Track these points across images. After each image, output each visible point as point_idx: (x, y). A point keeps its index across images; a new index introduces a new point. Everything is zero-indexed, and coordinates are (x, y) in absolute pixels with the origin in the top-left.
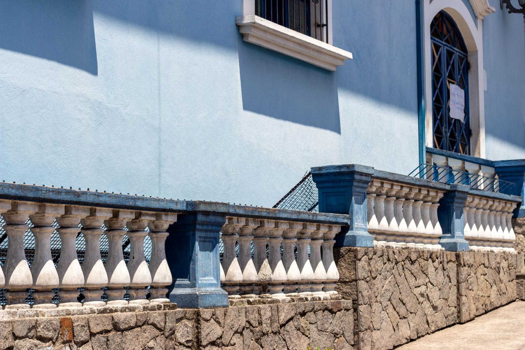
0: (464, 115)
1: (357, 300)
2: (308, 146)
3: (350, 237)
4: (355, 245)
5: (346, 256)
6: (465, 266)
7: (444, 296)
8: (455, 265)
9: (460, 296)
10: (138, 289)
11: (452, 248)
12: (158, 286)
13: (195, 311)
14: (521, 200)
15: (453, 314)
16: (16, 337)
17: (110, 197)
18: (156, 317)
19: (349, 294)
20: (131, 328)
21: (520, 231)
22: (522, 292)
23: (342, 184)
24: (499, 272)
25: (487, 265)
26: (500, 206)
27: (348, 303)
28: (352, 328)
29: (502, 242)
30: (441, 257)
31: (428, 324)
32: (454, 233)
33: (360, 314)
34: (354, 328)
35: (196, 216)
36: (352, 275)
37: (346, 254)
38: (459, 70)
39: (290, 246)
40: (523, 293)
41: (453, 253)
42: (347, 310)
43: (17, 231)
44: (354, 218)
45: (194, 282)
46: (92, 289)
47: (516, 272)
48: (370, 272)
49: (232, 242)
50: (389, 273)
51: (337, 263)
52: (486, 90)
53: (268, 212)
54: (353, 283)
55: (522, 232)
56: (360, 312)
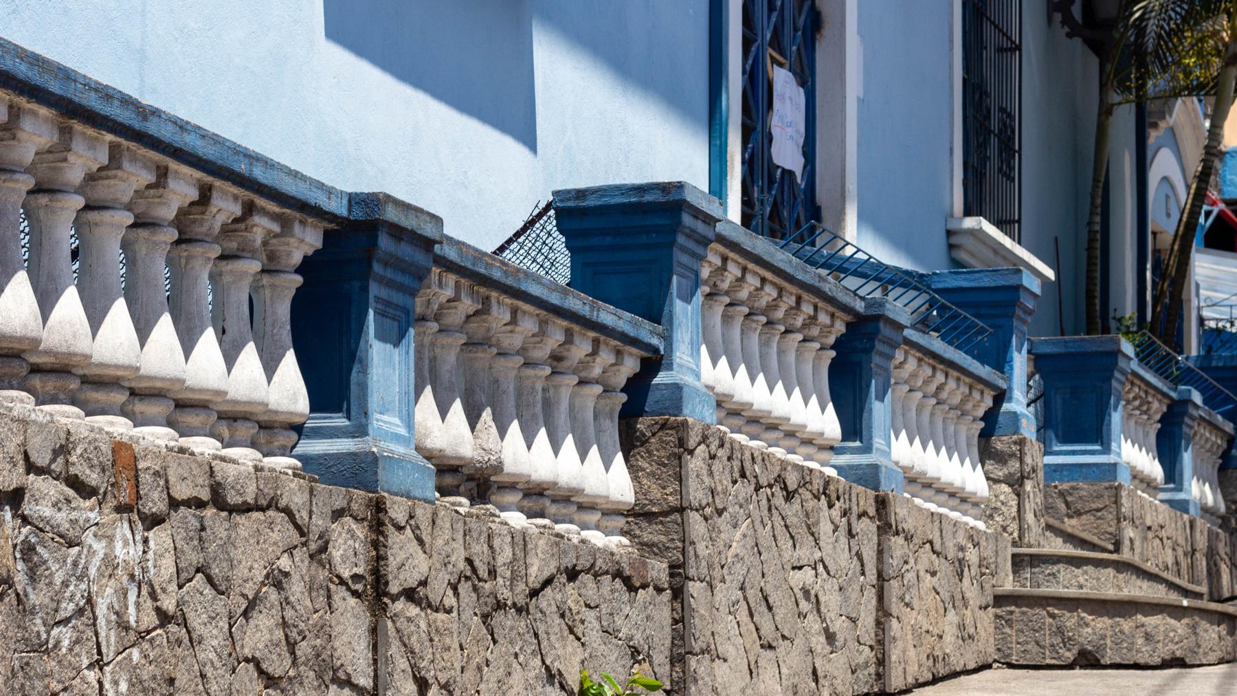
0: (802, 160)
1: (683, 565)
2: (465, 172)
3: (663, 387)
4: (678, 410)
5: (653, 440)
6: (897, 533)
7: (850, 609)
8: (873, 528)
9: (885, 616)
10: (235, 420)
11: (869, 477)
12: (275, 422)
13: (370, 499)
14: (1005, 386)
15: (866, 665)
16: (31, 468)
17: (203, 137)
18: (294, 494)
19: (659, 548)
20: (245, 509)
21: (1001, 474)
22: (1011, 643)
23: (643, 239)
24: (961, 576)
25: (938, 547)
26: (958, 392)
27: (658, 569)
28: (668, 642)
29: (958, 497)
30: (847, 497)
31: (816, 680)
32: (871, 438)
33: (690, 605)
34: (673, 642)
35: (377, 237)
36: (671, 494)
37: (654, 435)
38: (796, 30)
39: (533, 388)
40: (1014, 646)
41: (872, 493)
42: (659, 590)
43: (8, 188)
44: (675, 335)
45: (363, 420)
46: (147, 392)
47: (994, 586)
48: (712, 493)
49: (422, 340)
50: (742, 511)
51: (627, 460)
52: (862, 97)
53: (505, 272)
54: (673, 517)
55: (1005, 476)
56: (692, 600)
